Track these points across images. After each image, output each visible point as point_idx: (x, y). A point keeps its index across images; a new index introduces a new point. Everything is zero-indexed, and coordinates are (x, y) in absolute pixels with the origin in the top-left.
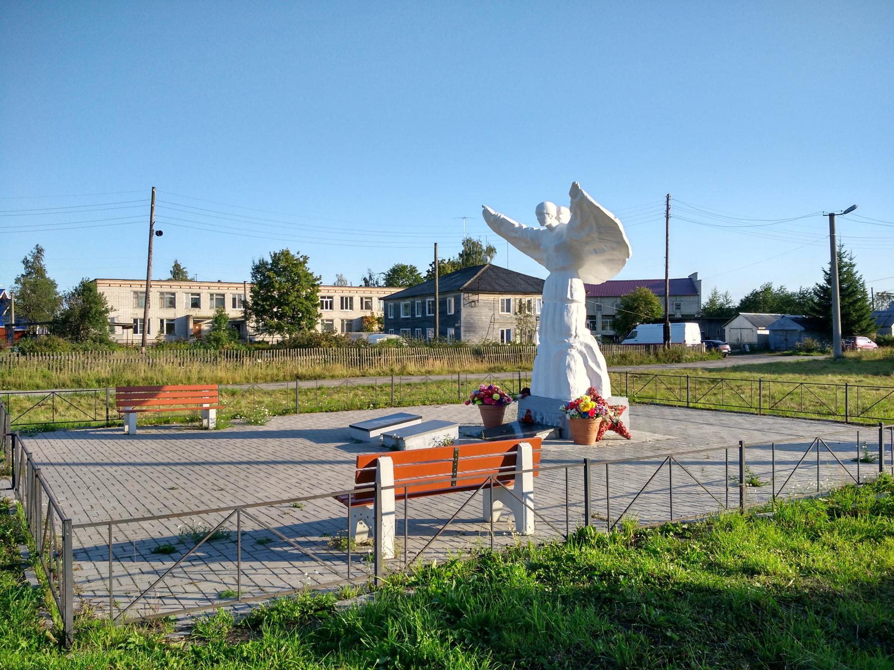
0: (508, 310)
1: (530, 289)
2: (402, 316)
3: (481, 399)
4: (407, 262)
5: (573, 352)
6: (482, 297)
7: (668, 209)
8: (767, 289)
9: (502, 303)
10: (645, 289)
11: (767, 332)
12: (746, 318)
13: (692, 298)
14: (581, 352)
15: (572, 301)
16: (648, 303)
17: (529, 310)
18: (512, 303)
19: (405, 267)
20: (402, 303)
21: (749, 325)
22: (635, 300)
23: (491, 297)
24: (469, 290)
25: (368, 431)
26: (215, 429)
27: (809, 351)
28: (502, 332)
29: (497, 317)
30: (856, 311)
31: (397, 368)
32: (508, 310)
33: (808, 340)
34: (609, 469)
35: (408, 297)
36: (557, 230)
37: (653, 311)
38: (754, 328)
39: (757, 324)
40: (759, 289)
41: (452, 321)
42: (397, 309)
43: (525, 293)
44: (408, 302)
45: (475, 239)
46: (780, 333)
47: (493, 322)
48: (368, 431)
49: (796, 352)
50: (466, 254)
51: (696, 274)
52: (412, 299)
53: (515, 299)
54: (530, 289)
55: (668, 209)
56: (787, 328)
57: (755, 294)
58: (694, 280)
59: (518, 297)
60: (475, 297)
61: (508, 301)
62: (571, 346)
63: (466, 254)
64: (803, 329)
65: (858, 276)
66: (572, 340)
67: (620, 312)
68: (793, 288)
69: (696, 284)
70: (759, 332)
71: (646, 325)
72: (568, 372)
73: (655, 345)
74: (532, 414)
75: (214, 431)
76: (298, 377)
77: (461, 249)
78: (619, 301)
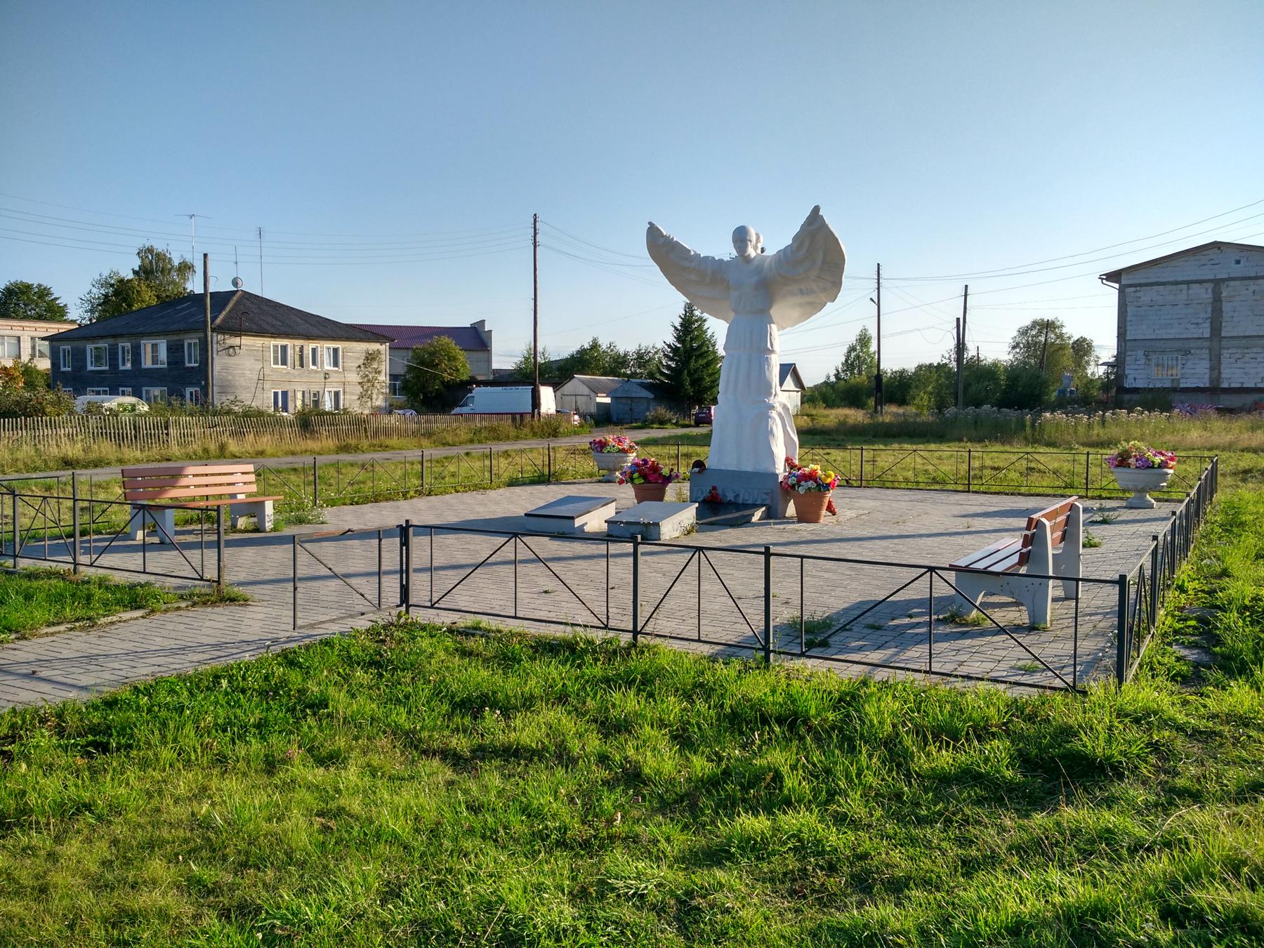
0: (284, 362)
1: (315, 331)
2: (90, 368)
3: (644, 476)
4: (33, 279)
5: (774, 414)
6: (246, 341)
7: (535, 234)
8: (595, 346)
9: (276, 352)
10: (445, 340)
11: (608, 400)
12: (583, 381)
13: (481, 355)
14: (779, 414)
15: (772, 352)
16: (452, 359)
17: (314, 363)
18: (290, 352)
19: (29, 287)
20: (90, 347)
21: (586, 391)
22: (432, 354)
23: (258, 342)
24: (220, 329)
25: (573, 518)
26: (272, 530)
27: (662, 423)
28: (276, 394)
29: (267, 371)
30: (710, 375)
31: (213, 447)
32: (284, 362)
33: (662, 411)
34: (384, 585)
35: (102, 337)
36: (755, 263)
37: (458, 370)
38: (593, 394)
39: (596, 390)
40: (587, 346)
41: (201, 376)
42: (79, 356)
43: (308, 337)
44: (103, 344)
45: (159, 247)
46: (624, 401)
47: (261, 379)
48: (573, 518)
49: (645, 425)
50: (146, 272)
51: (483, 321)
52: (111, 341)
53: (292, 344)
54: (315, 331)
55: (535, 234)
56: (633, 395)
57: (582, 352)
58: (480, 329)
59: (298, 343)
60: (235, 341)
61: (284, 348)
62: (773, 407)
63: (146, 272)
64: (651, 396)
65: (709, 333)
66: (772, 400)
67: (410, 369)
68: (627, 345)
69: (484, 336)
70: (599, 400)
71: (483, 389)
72: (771, 438)
73: (522, 415)
74: (720, 491)
75: (273, 534)
76: (293, 453)
77: (136, 263)
78: (410, 354)
